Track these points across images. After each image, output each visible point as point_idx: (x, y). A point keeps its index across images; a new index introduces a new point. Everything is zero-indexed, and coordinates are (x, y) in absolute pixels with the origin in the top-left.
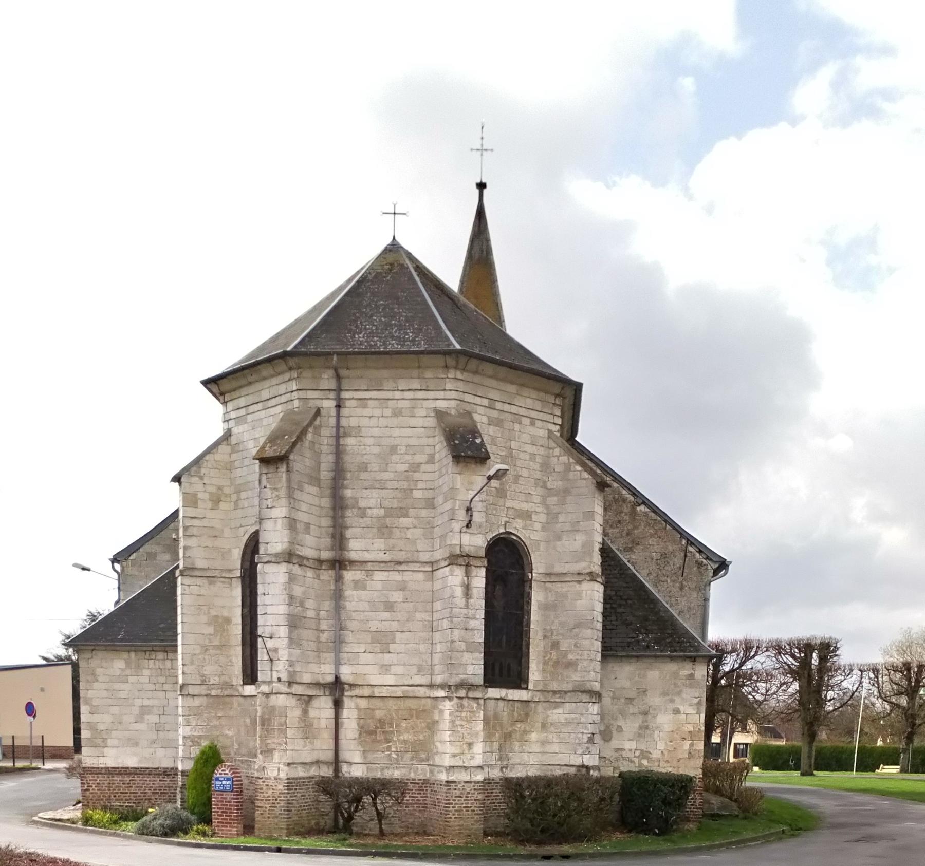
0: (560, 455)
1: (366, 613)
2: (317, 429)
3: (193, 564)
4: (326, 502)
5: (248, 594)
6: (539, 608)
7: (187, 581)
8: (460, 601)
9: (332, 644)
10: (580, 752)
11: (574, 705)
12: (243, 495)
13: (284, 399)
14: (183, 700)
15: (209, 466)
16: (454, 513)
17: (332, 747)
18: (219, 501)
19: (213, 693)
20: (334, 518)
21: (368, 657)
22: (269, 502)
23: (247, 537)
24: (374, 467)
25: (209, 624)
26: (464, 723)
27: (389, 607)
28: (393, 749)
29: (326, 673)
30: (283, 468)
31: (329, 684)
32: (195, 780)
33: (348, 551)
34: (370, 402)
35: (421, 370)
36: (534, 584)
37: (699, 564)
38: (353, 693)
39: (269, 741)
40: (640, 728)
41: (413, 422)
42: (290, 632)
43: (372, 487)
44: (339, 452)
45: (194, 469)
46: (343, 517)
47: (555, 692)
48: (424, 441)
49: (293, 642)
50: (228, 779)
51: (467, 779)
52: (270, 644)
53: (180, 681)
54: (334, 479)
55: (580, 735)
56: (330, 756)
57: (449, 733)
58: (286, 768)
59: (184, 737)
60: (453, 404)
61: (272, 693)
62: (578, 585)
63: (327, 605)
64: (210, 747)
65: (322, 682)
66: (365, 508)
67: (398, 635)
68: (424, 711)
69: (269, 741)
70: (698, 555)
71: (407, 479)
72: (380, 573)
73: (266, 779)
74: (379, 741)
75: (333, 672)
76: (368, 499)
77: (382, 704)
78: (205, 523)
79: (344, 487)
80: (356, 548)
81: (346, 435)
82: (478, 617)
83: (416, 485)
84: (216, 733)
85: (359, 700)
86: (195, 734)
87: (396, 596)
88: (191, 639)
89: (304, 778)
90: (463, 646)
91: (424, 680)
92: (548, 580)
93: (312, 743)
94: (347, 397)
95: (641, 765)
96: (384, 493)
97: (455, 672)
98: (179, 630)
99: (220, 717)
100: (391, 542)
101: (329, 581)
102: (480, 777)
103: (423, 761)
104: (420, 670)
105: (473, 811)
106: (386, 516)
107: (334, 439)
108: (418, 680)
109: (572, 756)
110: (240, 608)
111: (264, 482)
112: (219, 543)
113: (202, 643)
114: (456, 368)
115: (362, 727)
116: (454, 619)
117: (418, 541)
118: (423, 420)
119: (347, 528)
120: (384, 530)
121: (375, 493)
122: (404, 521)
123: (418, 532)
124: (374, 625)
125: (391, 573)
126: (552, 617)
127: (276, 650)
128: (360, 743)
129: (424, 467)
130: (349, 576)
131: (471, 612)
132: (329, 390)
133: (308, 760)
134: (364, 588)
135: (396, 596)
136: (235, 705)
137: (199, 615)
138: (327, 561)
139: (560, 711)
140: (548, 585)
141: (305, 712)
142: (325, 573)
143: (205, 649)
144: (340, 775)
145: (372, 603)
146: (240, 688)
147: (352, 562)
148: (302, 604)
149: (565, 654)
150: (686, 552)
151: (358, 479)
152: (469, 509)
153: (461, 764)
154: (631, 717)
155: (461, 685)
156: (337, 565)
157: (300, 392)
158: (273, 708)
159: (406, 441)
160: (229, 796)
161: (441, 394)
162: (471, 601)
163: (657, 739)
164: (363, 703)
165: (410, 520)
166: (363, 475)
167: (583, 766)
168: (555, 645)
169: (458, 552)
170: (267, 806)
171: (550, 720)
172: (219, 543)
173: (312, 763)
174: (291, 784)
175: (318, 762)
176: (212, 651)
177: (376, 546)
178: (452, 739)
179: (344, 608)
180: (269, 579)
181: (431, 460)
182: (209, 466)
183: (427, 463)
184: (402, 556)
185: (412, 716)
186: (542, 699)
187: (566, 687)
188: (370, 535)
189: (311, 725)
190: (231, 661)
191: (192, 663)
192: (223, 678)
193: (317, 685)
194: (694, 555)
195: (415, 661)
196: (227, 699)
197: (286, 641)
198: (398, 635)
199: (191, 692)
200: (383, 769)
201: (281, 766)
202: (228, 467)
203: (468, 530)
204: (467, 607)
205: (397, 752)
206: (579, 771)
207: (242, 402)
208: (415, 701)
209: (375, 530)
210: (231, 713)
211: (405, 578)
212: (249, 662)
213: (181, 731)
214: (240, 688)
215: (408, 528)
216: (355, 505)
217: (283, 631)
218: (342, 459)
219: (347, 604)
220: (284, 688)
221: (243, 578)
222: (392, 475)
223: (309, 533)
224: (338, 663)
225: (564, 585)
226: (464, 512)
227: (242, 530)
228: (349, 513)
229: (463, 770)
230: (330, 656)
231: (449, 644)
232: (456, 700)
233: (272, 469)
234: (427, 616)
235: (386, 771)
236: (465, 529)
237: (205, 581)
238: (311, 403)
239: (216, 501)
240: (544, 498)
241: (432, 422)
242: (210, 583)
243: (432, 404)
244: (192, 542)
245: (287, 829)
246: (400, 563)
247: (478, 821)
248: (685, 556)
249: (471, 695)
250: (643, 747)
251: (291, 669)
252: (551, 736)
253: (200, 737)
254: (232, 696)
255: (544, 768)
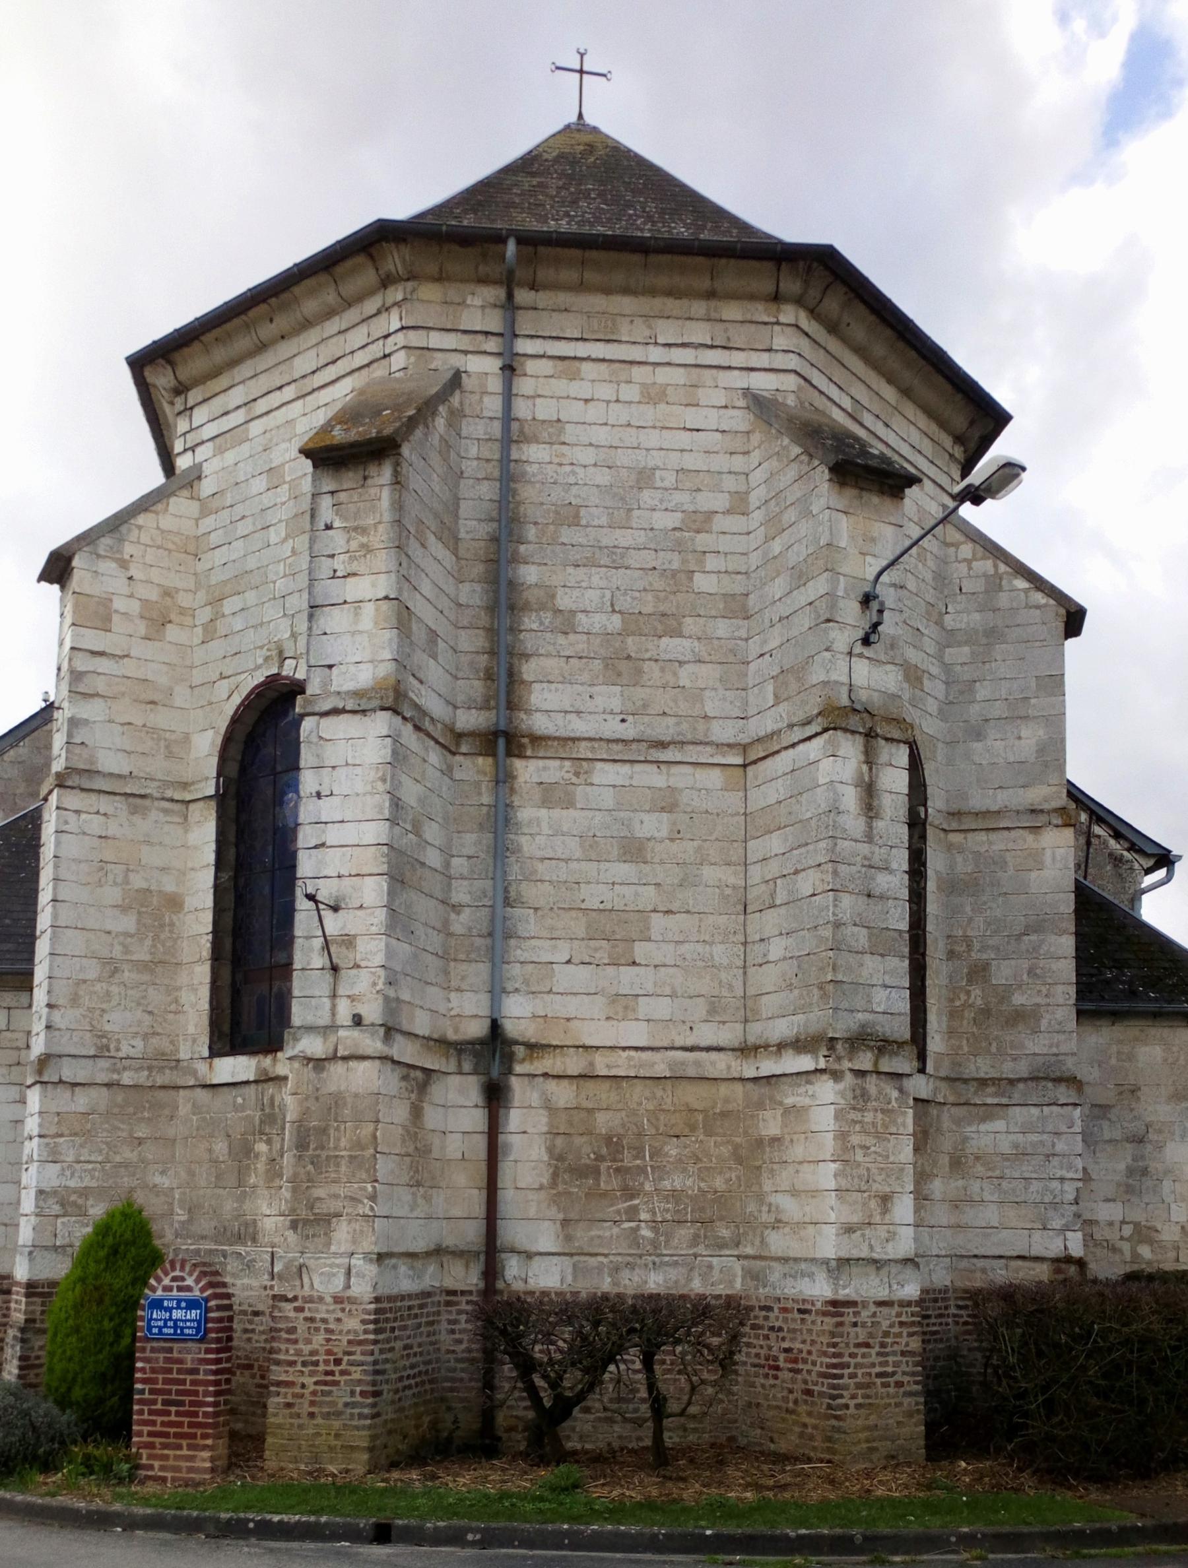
0: (974, 558)
1: (574, 865)
2: (456, 416)
3: (92, 760)
4: (473, 594)
5: (232, 837)
6: (938, 888)
7: (74, 800)
8: (854, 823)
9: (479, 942)
10: (1057, 1223)
11: (1035, 1111)
12: (229, 606)
13: (361, 358)
14: (43, 1096)
15: (145, 538)
16: (833, 606)
17: (479, 1210)
18: (165, 622)
19: (127, 1078)
20: (492, 632)
21: (579, 976)
22: (340, 564)
23: (237, 700)
24: (596, 515)
25: (124, 909)
26: (869, 1141)
27: (634, 850)
28: (644, 1216)
29: (468, 1015)
30: (385, 474)
31: (472, 1043)
32: (78, 1307)
33: (528, 712)
34: (586, 367)
35: (713, 303)
36: (930, 831)
37: (1117, 860)
38: (538, 1067)
39: (319, 1192)
40: (1130, 1172)
41: (692, 417)
42: (391, 893)
43: (591, 563)
44: (508, 476)
45: (106, 541)
46: (514, 630)
47: (983, 1082)
48: (720, 462)
49: (398, 922)
50: (192, 1304)
51: (883, 1294)
52: (333, 924)
53: (38, 1047)
54: (495, 539)
55: (1055, 1184)
56: (471, 1233)
57: (833, 1166)
58: (372, 1270)
59: (40, 1192)
60: (791, 382)
61: (334, 1057)
62: (1030, 838)
63: (471, 842)
64: (125, 1215)
65: (452, 1036)
66: (573, 613)
67: (657, 921)
68: (724, 1114)
69: (319, 1192)
70: (1112, 842)
71: (679, 547)
72: (608, 767)
73: (310, 1300)
74: (604, 1194)
75: (485, 1011)
76: (576, 589)
77: (614, 1097)
78: (129, 668)
79: (515, 559)
80: (549, 705)
81: (525, 439)
82: (894, 866)
83: (701, 562)
84: (127, 1181)
85: (551, 1086)
86: (72, 1184)
87: (651, 825)
88: (74, 942)
89: (410, 1296)
90: (861, 937)
91: (728, 1035)
92: (954, 826)
93: (428, 1199)
94: (530, 351)
95: (1136, 1256)
96: (619, 578)
97: (845, 1005)
98: (44, 921)
99: (140, 1141)
100: (640, 693)
101: (478, 784)
102: (911, 1291)
103: (722, 1246)
104: (714, 1010)
105: (899, 1384)
106: (625, 633)
107: (496, 446)
108: (707, 1034)
109: (1037, 1235)
110: (211, 871)
111: (326, 510)
112: (161, 719)
113: (105, 953)
114: (799, 301)
115: (561, 1158)
116: (842, 868)
117: (707, 693)
118: (716, 409)
119: (527, 656)
120: (620, 665)
121: (597, 577)
122: (671, 646)
123: (708, 674)
124: (593, 896)
125: (638, 767)
126: (968, 909)
127: (349, 941)
128: (555, 1200)
129: (720, 522)
130: (527, 771)
131: (879, 854)
132: (487, 333)
133: (420, 1246)
134: (569, 804)
135: (651, 825)
136: (184, 1109)
137: (100, 884)
138: (472, 734)
139: (1000, 1125)
140: (955, 838)
141: (417, 1112)
142: (467, 762)
143: (112, 968)
144: (500, 1285)
145: (589, 841)
146: (202, 1067)
147: (537, 740)
148: (417, 830)
149: (1004, 995)
150: (1089, 836)
151: (554, 541)
152: (867, 600)
153: (864, 1253)
154: (1109, 1148)
155: (859, 1040)
156: (501, 742)
157: (411, 333)
158: (338, 1100)
159: (674, 460)
160: (192, 1354)
161: (763, 360)
162: (879, 825)
163: (1169, 1199)
164: (563, 1094)
165: (686, 643)
166: (567, 535)
167: (1068, 1260)
168: (979, 973)
169: (845, 701)
170: (309, 1381)
171: (973, 1147)
172: (161, 719)
173: (428, 1254)
174: (387, 1312)
175: (438, 1252)
176: (127, 975)
177: (600, 702)
178: (844, 1183)
179: (519, 850)
180: (332, 755)
181: (739, 505)
182: (145, 538)
183: (728, 512)
184: (664, 729)
185: (693, 1128)
186: (951, 1099)
187: (1009, 1069)
188: (586, 677)
189: (427, 1150)
190: (176, 1001)
191: (75, 1001)
192: (154, 1041)
193: (442, 1044)
194: (1105, 843)
195: (704, 985)
196: (161, 1095)
197: (381, 915)
198: (657, 921)
199: (67, 1074)
200: (617, 1269)
201: (357, 1262)
202: (191, 548)
203: (867, 652)
204: (869, 838)
205: (654, 1224)
206: (1058, 1271)
207: (237, 396)
208: (703, 1090)
209: (597, 665)
210: (171, 1132)
211: (672, 782)
212: (226, 1002)
213: (31, 1178)
214: (202, 1067)
215: (681, 663)
216: (548, 602)
217: (373, 891)
218: (515, 492)
219: (524, 840)
220: (372, 1044)
221: (220, 798)
222: (641, 538)
223: (434, 657)
224: (497, 991)
225: (993, 836)
226: (855, 606)
227: (223, 687)
228: (530, 622)
229: (871, 1269)
230: (478, 972)
231: (827, 932)
232: (849, 1078)
233: (350, 478)
234: (731, 876)
235: (625, 1274)
236: (858, 648)
237: (120, 804)
238: (438, 361)
239: (158, 620)
240: (942, 647)
241: (739, 420)
242: (134, 811)
243: (739, 380)
244: (92, 710)
245: (371, 1449)
246: (662, 745)
247: (910, 1414)
248: (1088, 843)
249: (886, 1065)
250: (1138, 1215)
251: (391, 993)
252: (975, 1186)
253: (85, 1192)
254: (177, 1088)
255: (964, 1264)
